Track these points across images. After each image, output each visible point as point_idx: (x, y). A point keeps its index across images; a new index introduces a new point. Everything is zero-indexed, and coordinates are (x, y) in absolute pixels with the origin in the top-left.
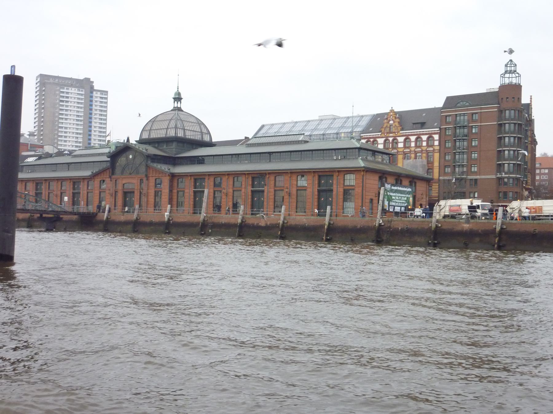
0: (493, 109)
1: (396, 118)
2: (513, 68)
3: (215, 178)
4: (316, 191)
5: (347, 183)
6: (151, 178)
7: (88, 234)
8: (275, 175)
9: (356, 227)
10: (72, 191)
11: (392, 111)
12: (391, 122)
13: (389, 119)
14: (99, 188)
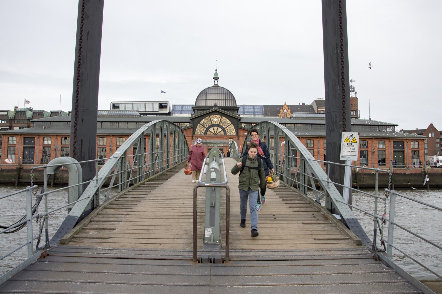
0: (181, 107)
1: (288, 109)
2: (353, 90)
3: (44, 138)
4: (22, 147)
5: (10, 142)
6: (241, 138)
7: (429, 192)
8: (43, 137)
9: (12, 169)
10: (22, 146)
11: (285, 104)
12: (285, 111)
13: (284, 109)
14: (60, 144)
